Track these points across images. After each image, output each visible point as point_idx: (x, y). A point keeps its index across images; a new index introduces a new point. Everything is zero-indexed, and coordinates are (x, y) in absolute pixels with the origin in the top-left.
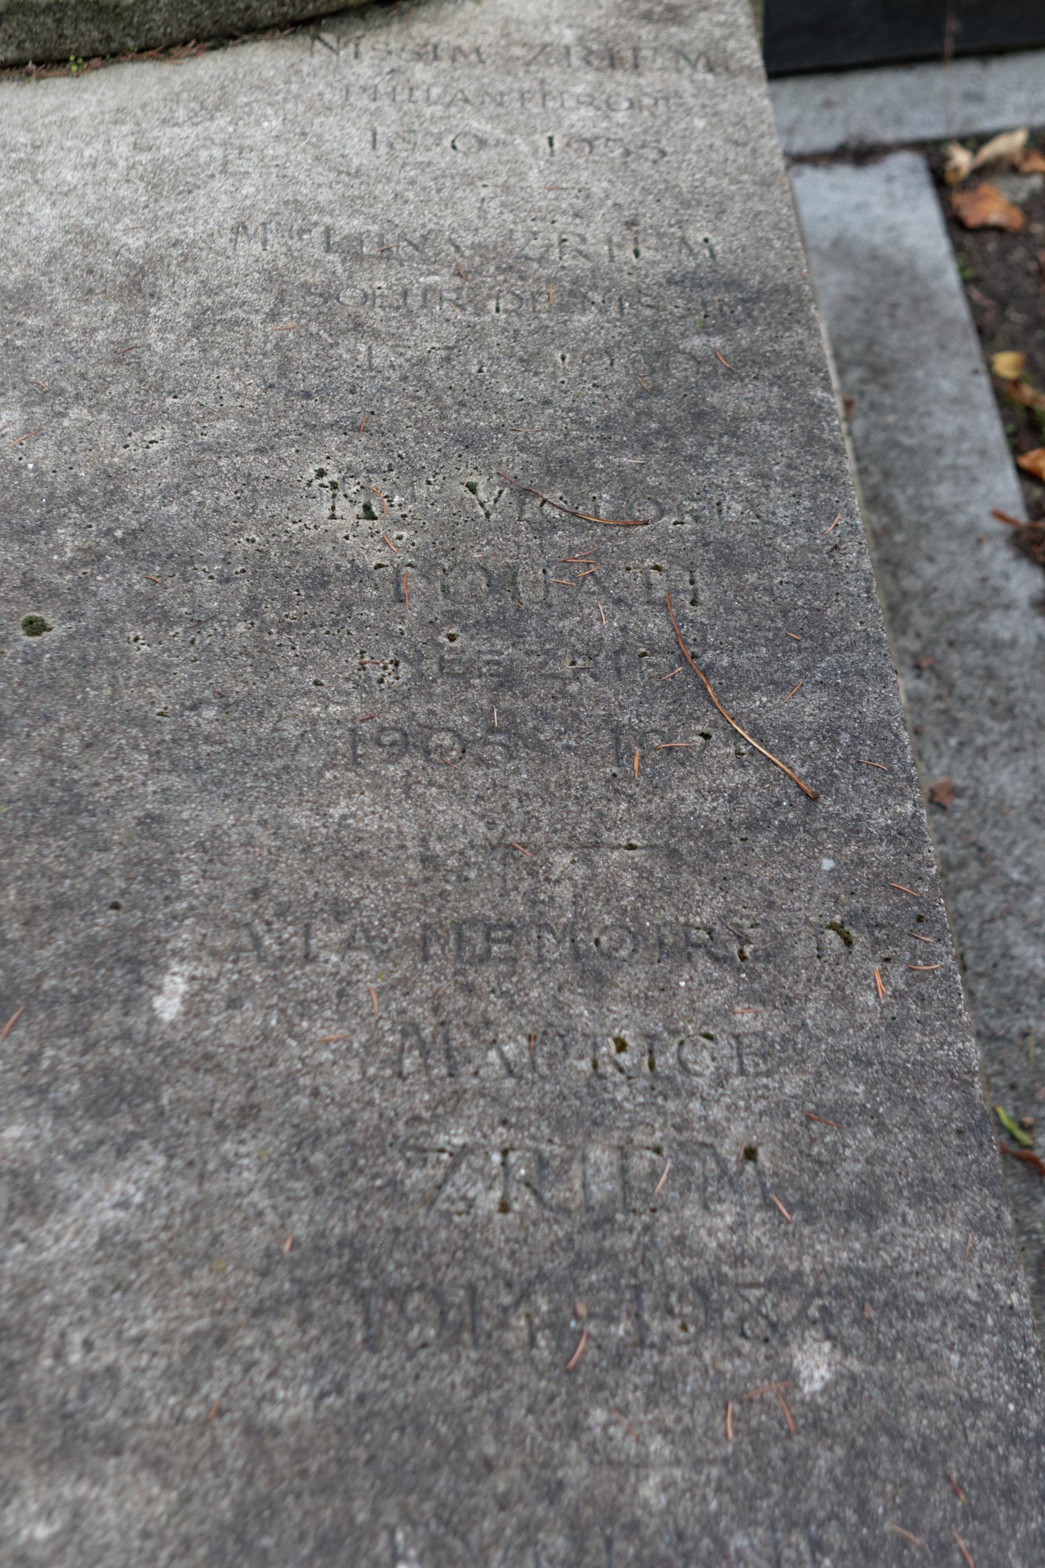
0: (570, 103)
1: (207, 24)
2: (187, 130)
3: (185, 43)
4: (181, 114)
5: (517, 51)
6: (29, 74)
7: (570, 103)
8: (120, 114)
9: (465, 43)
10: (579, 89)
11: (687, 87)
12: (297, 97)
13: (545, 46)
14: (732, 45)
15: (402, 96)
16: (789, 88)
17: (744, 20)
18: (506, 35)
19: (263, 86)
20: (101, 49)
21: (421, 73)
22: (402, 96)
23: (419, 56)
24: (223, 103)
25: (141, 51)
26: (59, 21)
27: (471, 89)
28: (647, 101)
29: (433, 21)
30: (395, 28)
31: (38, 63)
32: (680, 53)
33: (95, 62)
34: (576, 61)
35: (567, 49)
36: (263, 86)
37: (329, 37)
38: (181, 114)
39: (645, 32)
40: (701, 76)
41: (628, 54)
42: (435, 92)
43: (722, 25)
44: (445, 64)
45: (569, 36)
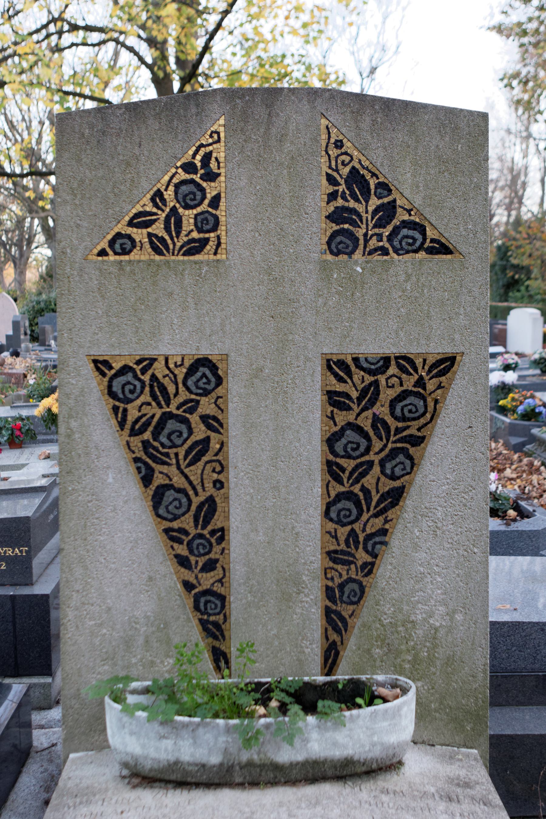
0: (439, 812)
1: (310, 775)
2: (306, 811)
3: (301, 781)
4: (303, 805)
5: (416, 793)
6: (245, 788)
7: (439, 812)
8: (281, 804)
9: (397, 789)
10: (441, 808)
11: (478, 810)
12: (344, 803)
13: (425, 793)
14: (490, 797)
15: (380, 805)
16: (497, 710)
17: (365, 610)
18: (411, 787)
19: (330, 798)
20: (272, 781)
21: (385, 798)
22: (380, 805)
23: (382, 792)
24: (317, 803)
25: (285, 783)
26: (261, 771)
27: (403, 805)
28: (466, 814)
29: (385, 781)
30: (372, 782)
31: (249, 784)
32: (473, 798)
33: (269, 785)
34: (437, 798)
35: (433, 795)
36: (330, 798)
37: (350, 783)
38: (303, 805)
39: (459, 790)
40: (482, 806)
41: (455, 798)
42: (391, 805)
43: (486, 790)
44: (392, 795)
45: (433, 790)
